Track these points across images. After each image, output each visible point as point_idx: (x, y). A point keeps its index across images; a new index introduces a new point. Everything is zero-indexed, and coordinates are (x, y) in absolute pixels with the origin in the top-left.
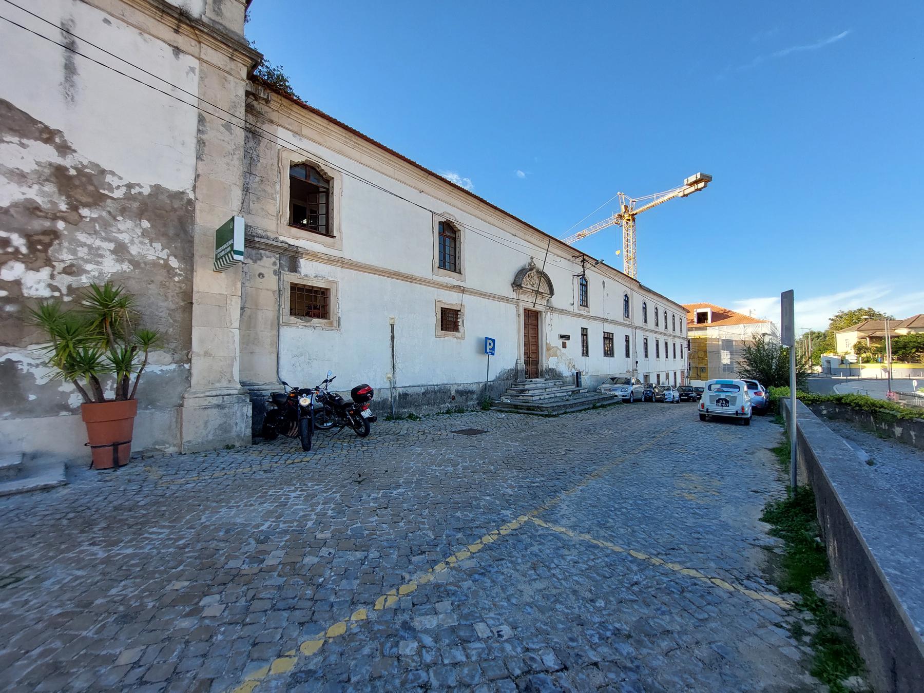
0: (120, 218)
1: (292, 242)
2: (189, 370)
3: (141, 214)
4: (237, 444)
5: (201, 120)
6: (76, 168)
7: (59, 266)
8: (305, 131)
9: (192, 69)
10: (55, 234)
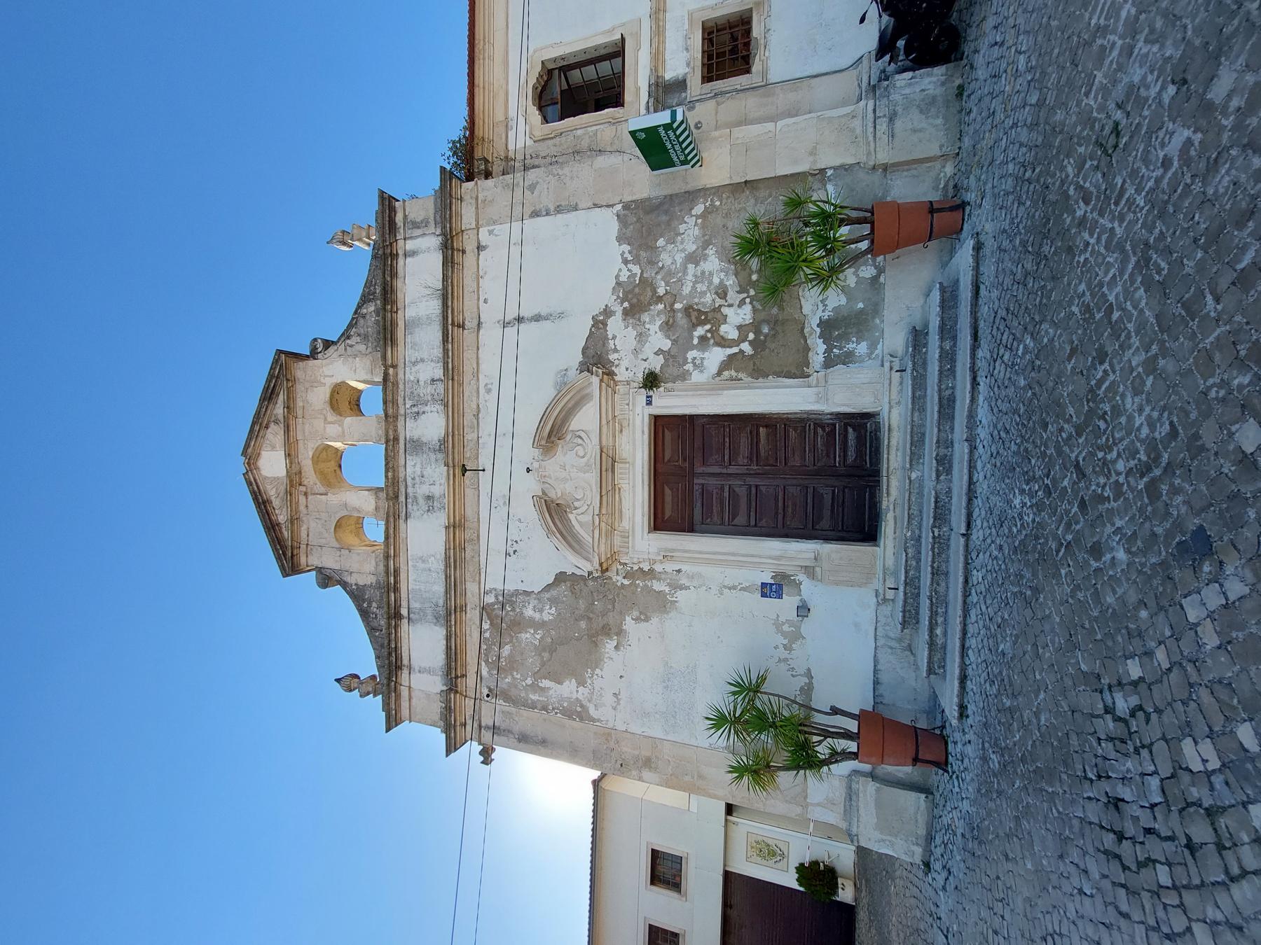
0: (660, 264)
1: (644, 96)
2: (835, 168)
3: (653, 248)
4: (958, 82)
5: (535, 214)
6: (622, 303)
7: (719, 302)
8: (500, 116)
9: (491, 232)
10: (688, 310)
